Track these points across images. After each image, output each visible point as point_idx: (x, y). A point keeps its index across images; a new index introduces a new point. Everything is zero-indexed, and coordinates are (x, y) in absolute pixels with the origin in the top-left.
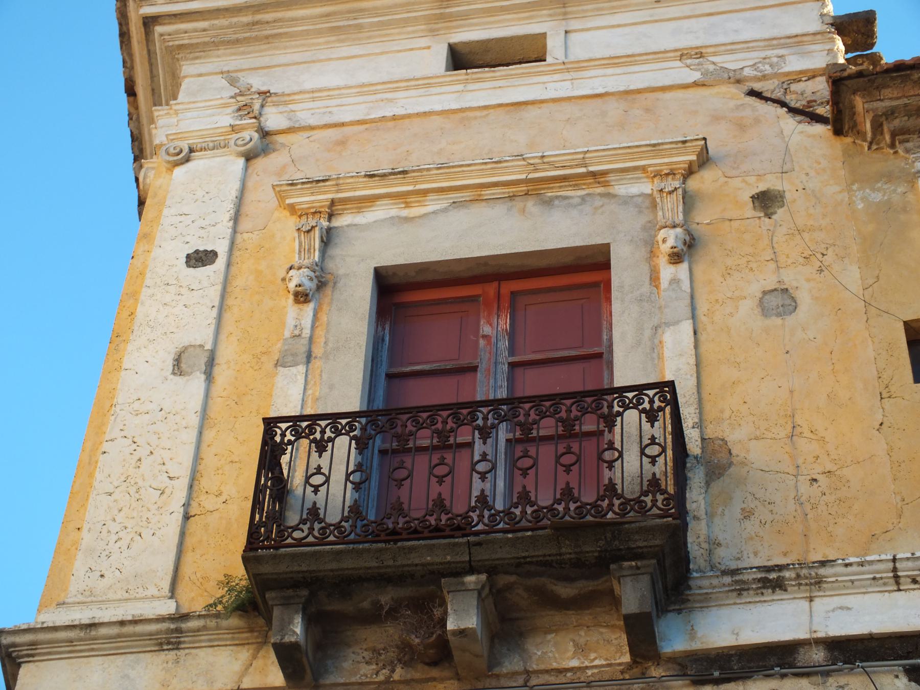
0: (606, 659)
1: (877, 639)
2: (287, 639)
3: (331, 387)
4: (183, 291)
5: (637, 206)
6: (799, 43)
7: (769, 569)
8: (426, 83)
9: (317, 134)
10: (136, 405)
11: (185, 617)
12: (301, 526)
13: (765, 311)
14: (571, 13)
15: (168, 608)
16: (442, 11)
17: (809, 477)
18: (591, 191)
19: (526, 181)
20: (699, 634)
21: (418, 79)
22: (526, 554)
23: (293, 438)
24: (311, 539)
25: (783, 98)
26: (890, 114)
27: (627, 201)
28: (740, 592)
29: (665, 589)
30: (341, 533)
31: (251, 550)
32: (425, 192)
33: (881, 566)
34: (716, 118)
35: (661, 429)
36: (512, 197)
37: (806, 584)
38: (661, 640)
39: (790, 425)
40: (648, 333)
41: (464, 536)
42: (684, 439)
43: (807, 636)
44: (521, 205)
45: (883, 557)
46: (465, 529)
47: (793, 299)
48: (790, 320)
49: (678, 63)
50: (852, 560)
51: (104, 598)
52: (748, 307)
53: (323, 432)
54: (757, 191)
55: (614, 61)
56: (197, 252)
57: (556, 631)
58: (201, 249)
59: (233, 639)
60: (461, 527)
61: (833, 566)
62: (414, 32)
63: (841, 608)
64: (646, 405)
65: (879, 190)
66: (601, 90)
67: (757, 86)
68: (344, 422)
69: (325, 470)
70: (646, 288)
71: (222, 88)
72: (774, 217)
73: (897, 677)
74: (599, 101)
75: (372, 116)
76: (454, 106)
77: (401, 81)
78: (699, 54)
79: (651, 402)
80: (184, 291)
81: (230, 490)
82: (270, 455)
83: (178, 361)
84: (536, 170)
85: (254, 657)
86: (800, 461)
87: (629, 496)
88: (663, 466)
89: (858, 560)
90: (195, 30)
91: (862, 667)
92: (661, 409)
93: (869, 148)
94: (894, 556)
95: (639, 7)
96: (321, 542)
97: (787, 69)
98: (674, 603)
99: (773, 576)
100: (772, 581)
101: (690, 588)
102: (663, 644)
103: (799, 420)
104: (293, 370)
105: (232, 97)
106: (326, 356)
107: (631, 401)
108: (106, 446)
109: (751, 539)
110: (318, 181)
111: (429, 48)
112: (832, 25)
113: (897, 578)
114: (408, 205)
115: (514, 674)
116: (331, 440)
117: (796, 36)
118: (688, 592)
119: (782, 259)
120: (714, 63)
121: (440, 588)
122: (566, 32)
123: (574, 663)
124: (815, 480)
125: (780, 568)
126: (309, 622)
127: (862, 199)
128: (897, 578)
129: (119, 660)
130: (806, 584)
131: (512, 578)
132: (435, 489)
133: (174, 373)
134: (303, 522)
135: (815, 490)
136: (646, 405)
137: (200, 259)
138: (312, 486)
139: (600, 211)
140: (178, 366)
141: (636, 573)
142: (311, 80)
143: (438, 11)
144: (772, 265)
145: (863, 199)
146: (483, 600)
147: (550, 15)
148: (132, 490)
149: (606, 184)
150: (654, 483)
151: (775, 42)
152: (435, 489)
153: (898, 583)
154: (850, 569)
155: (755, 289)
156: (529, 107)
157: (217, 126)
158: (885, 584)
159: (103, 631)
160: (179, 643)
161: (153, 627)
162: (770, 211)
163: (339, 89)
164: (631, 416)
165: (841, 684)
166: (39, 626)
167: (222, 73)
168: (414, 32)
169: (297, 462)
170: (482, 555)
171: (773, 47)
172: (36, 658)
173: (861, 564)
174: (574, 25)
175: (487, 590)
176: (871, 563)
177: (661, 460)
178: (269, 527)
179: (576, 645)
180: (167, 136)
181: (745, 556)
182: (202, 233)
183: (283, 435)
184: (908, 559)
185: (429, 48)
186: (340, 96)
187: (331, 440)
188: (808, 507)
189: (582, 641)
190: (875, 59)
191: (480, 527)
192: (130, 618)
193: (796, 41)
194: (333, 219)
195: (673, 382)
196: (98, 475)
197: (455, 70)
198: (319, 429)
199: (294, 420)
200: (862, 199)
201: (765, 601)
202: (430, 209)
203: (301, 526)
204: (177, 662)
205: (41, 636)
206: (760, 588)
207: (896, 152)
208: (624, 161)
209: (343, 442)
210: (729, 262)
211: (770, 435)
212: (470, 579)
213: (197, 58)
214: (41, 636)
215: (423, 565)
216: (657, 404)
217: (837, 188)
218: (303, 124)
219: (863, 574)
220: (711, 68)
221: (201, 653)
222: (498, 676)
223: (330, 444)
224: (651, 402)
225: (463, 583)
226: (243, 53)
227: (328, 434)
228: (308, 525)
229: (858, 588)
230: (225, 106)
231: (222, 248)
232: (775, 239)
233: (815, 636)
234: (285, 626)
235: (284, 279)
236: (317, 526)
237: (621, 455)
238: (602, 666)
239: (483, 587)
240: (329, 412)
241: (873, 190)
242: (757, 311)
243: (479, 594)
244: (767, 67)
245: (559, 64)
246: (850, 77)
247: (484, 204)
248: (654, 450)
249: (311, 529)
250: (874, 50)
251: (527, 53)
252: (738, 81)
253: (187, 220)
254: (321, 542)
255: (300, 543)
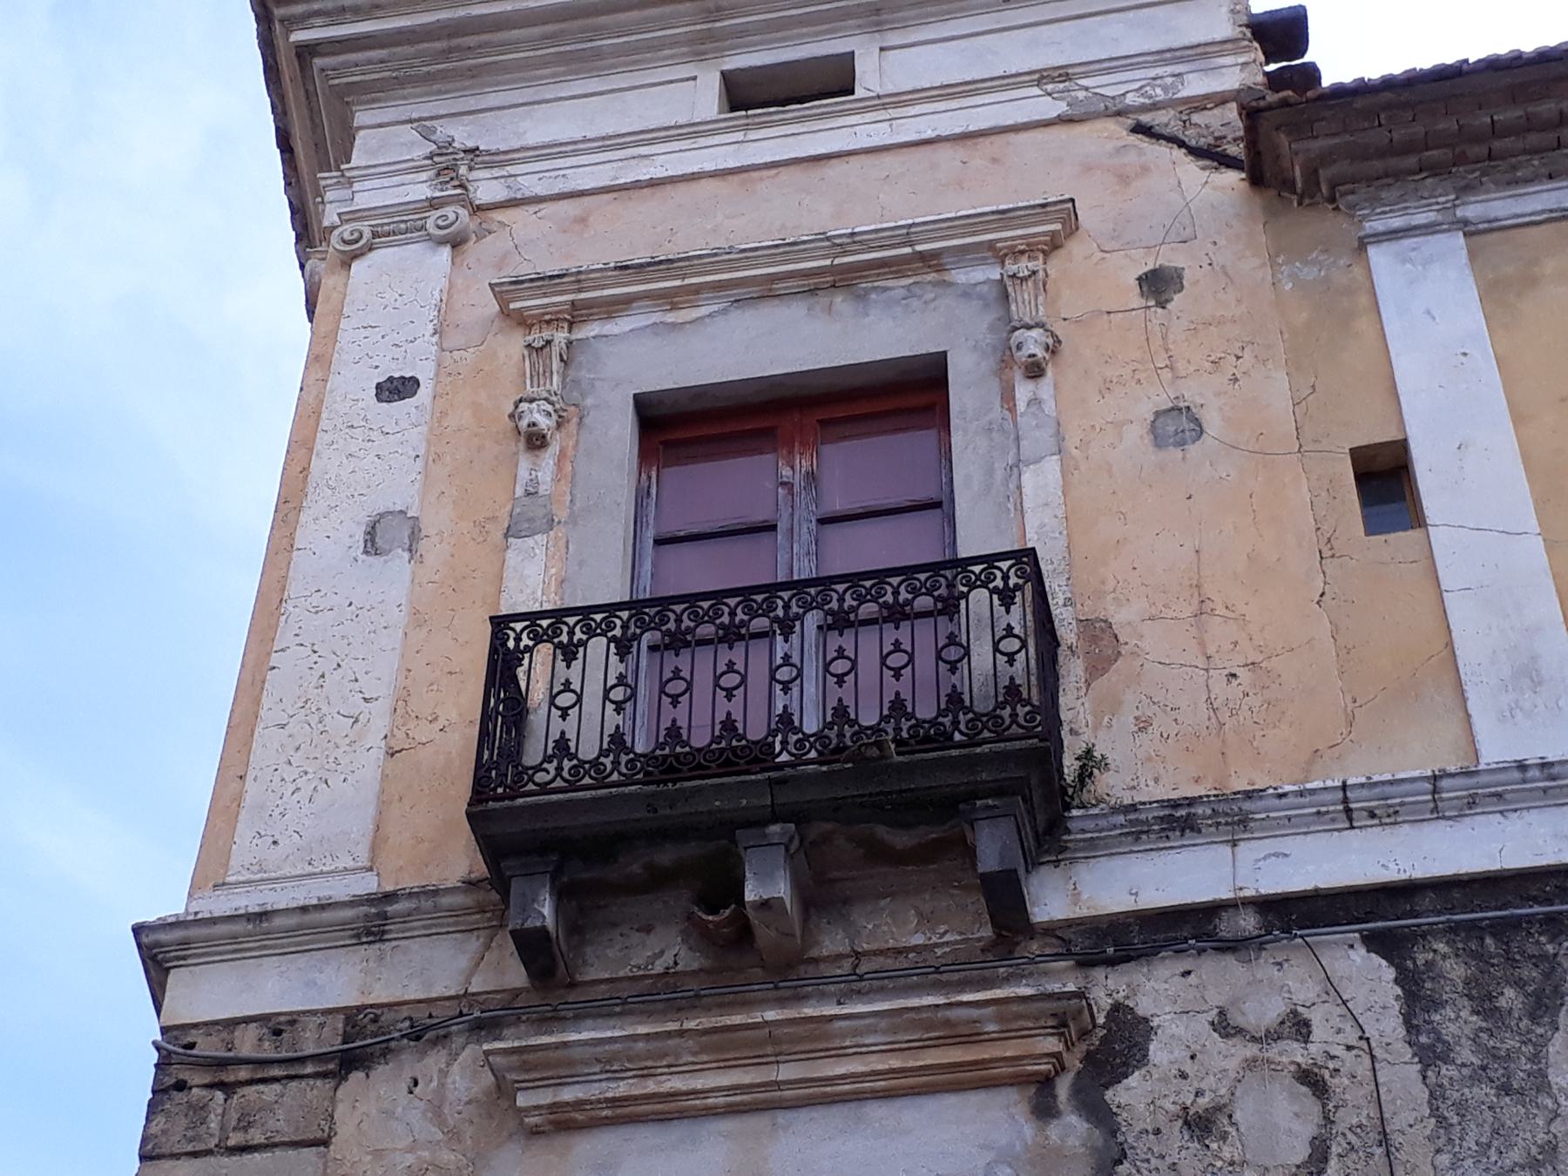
0: (961, 933)
1: (1326, 896)
2: (529, 924)
3: (581, 564)
4: (374, 435)
5: (981, 297)
6: (1205, 56)
7: (1175, 804)
8: (691, 131)
9: (548, 209)
10: (316, 600)
11: (390, 897)
12: (545, 765)
13: (1159, 440)
14: (886, 22)
15: (368, 884)
16: (710, 25)
17: (1226, 672)
18: (918, 279)
19: (830, 270)
20: (1085, 896)
21: (681, 127)
22: (847, 793)
23: (531, 643)
24: (559, 783)
25: (1181, 136)
26: (1325, 159)
27: (967, 293)
28: (1137, 836)
29: (1036, 833)
30: (598, 772)
31: (480, 802)
32: (697, 290)
33: (1328, 797)
34: (1088, 168)
35: (1018, 617)
36: (813, 291)
37: (1227, 824)
38: (1033, 904)
39: (1195, 601)
40: (999, 474)
41: (763, 770)
42: (1052, 622)
43: (1231, 895)
44: (826, 300)
45: (1329, 783)
46: (764, 761)
47: (1197, 421)
48: (1193, 450)
49: (1036, 91)
50: (1288, 788)
51: (278, 875)
52: (1136, 434)
53: (571, 633)
54: (1146, 269)
55: (948, 92)
56: (391, 379)
57: (892, 895)
58: (397, 375)
59: (456, 924)
60: (760, 755)
61: (1261, 798)
62: (672, 57)
63: (1276, 855)
64: (999, 583)
65: (1314, 262)
66: (930, 134)
67: (1145, 118)
68: (598, 617)
69: (576, 686)
70: (997, 411)
71: (413, 143)
72: (1169, 306)
73: (1352, 946)
74: (929, 148)
75: (622, 181)
76: (731, 164)
77: (659, 130)
78: (1063, 74)
79: (1006, 578)
80: (374, 435)
81: (449, 713)
82: (502, 667)
83: (371, 534)
84: (845, 253)
85: (488, 947)
86: (1211, 650)
87: (980, 707)
88: (1022, 669)
89: (1295, 788)
90: (370, 62)
91: (1302, 937)
92: (1017, 587)
93: (1300, 204)
94: (1344, 783)
95: (986, 8)
96: (572, 787)
97: (1185, 93)
98: (1048, 852)
99: (1182, 812)
100: (1177, 822)
101: (1068, 832)
102: (1036, 909)
103: (1208, 590)
104: (530, 541)
105: (427, 158)
106: (573, 519)
107: (978, 577)
108: (275, 659)
109: (1149, 759)
110: (552, 277)
111: (694, 78)
112: (1247, 26)
113: (1348, 811)
114: (674, 307)
115: (840, 957)
116: (529, 649)
117: (1199, 45)
118: (1065, 837)
119: (1180, 365)
120: (1087, 89)
121: (734, 842)
122: (882, 49)
123: (918, 939)
124: (1234, 675)
125: (1191, 802)
126: (562, 896)
127: (1289, 276)
128: (1348, 811)
129: (302, 960)
130: (1227, 824)
131: (829, 826)
132: (723, 706)
133: (366, 552)
134: (548, 759)
135: (1234, 690)
136: (999, 583)
137: (396, 389)
138: (737, 672)
139: (932, 306)
140: (372, 543)
141: (993, 815)
142: (539, 127)
143: (704, 26)
144: (1167, 375)
145: (1293, 277)
146: (792, 857)
147: (859, 26)
148: (314, 720)
149: (940, 269)
150: (1013, 690)
151: (1168, 55)
152: (723, 706)
153: (1350, 820)
154: (1284, 800)
155: (1146, 411)
156: (834, 161)
157: (407, 199)
158: (1333, 820)
159: (278, 922)
160: (384, 932)
161: (348, 913)
162: (1164, 297)
163: (575, 143)
164: (980, 597)
165: (1279, 960)
166: (191, 918)
167: (410, 121)
168: (672, 57)
169: (538, 673)
170: (786, 797)
171: (1167, 62)
172: (190, 961)
173: (1301, 794)
174: (893, 38)
175: (796, 842)
176: (1313, 792)
177: (1021, 657)
178: (503, 768)
179: (920, 915)
180: (339, 215)
181: (1142, 785)
182: (398, 353)
183: (518, 639)
184: (1362, 785)
185: (694, 78)
186: (575, 153)
187: (583, 644)
188: (1224, 715)
189: (927, 908)
190: (1311, 74)
191: (784, 757)
192: (315, 902)
193: (1200, 53)
194: (575, 330)
195: (1033, 549)
196: (266, 701)
197: (732, 110)
198: (565, 629)
199: (532, 617)
200: (1289, 276)
201: (1172, 848)
202: (704, 311)
203: (545, 765)
204: (381, 958)
205: (193, 932)
206: (1163, 830)
207: (1337, 209)
208: (963, 236)
209: (598, 645)
210: (1110, 372)
211: (1171, 614)
212: (775, 828)
213: (373, 101)
214: (193, 932)
215: (709, 812)
216: (1013, 581)
217: (1257, 262)
218: (528, 194)
219: (1304, 807)
220: (1081, 95)
221: (414, 945)
222: (815, 961)
223: (581, 650)
224: (1006, 578)
225: (765, 836)
226: (440, 92)
227: (579, 635)
228: (555, 763)
229: (1297, 826)
230: (419, 169)
231: (425, 373)
232: (1171, 337)
233: (1242, 894)
234: (527, 907)
235: (512, 416)
236: (567, 764)
237: (967, 653)
238: (957, 942)
239: (791, 840)
240: (579, 605)
241: (1306, 263)
242: (1148, 439)
243: (787, 850)
244: (1158, 91)
245: (872, 98)
246: (1270, 108)
247: (776, 301)
248: (1011, 645)
249: (559, 769)
250: (1307, 59)
251: (831, 82)
252: (1119, 114)
253: (375, 335)
254: (572, 787)
255: (544, 789)
